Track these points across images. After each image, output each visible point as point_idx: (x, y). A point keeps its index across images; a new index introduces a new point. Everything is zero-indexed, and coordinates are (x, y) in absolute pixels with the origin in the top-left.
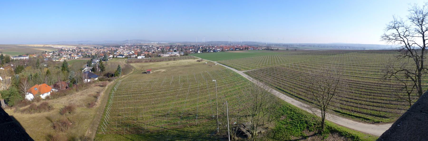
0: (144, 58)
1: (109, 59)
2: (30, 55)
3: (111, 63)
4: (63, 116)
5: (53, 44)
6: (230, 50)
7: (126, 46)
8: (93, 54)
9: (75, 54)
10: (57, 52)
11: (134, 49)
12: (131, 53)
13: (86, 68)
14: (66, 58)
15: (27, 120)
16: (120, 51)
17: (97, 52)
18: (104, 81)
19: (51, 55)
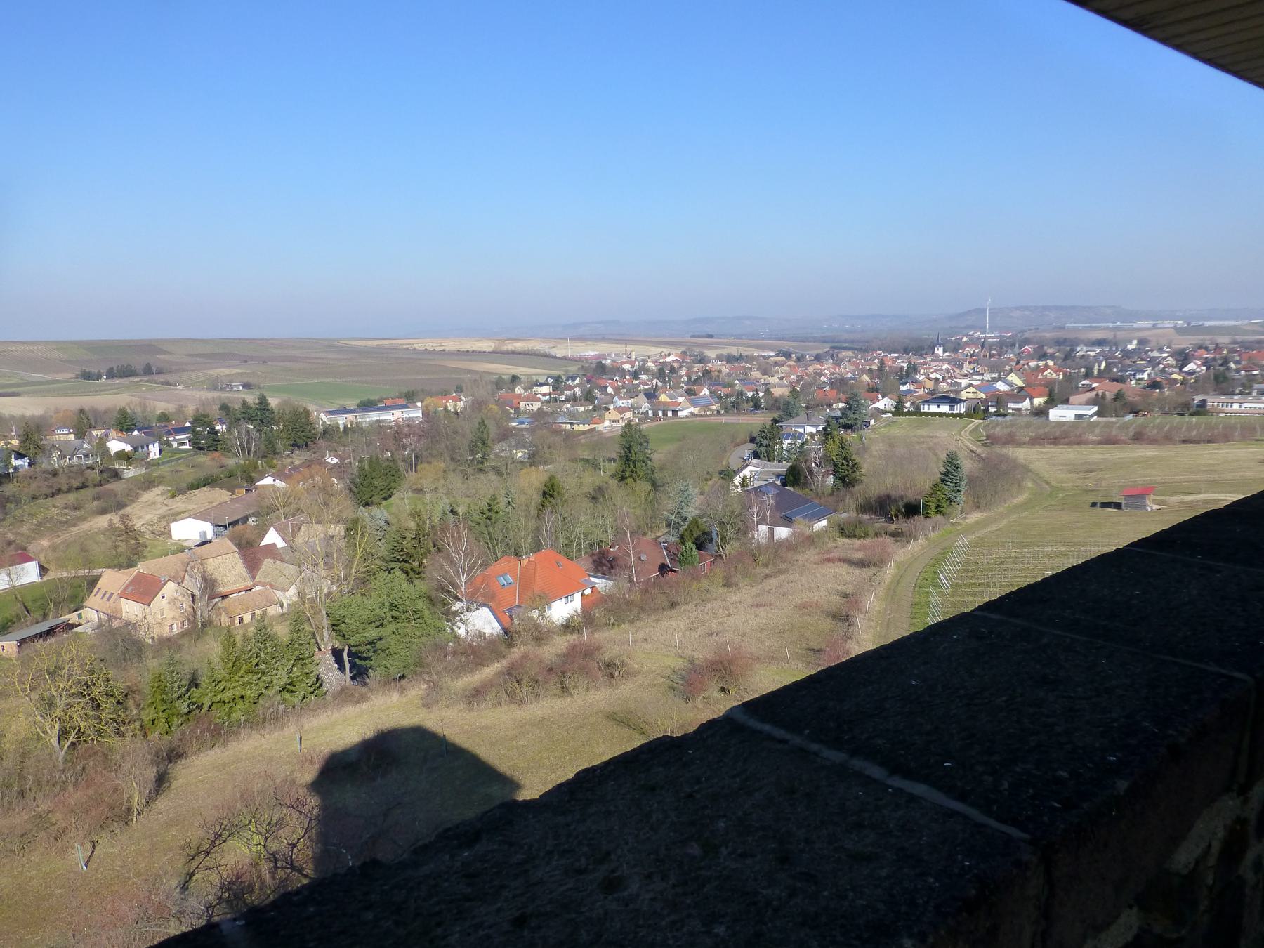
0: (1092, 416)
1: (872, 422)
2: (428, 401)
3: (891, 443)
4: (690, 705)
5: (545, 339)
7: (967, 344)
8: (777, 392)
9: (680, 391)
10: (574, 379)
11: (1018, 363)
12: (1001, 387)
13: (749, 468)
14: (629, 415)
15: (512, 738)
16: (932, 372)
17: (799, 379)
18: (866, 535)
19: (544, 395)
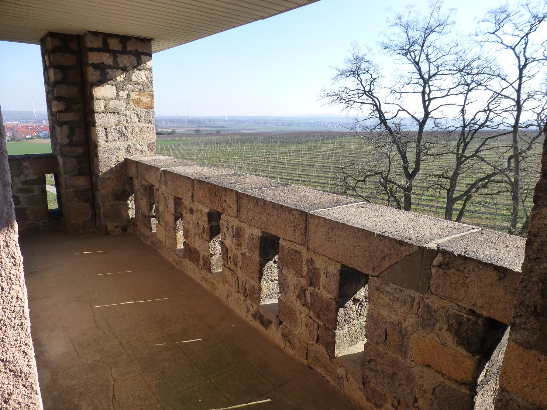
6: (40, 137)
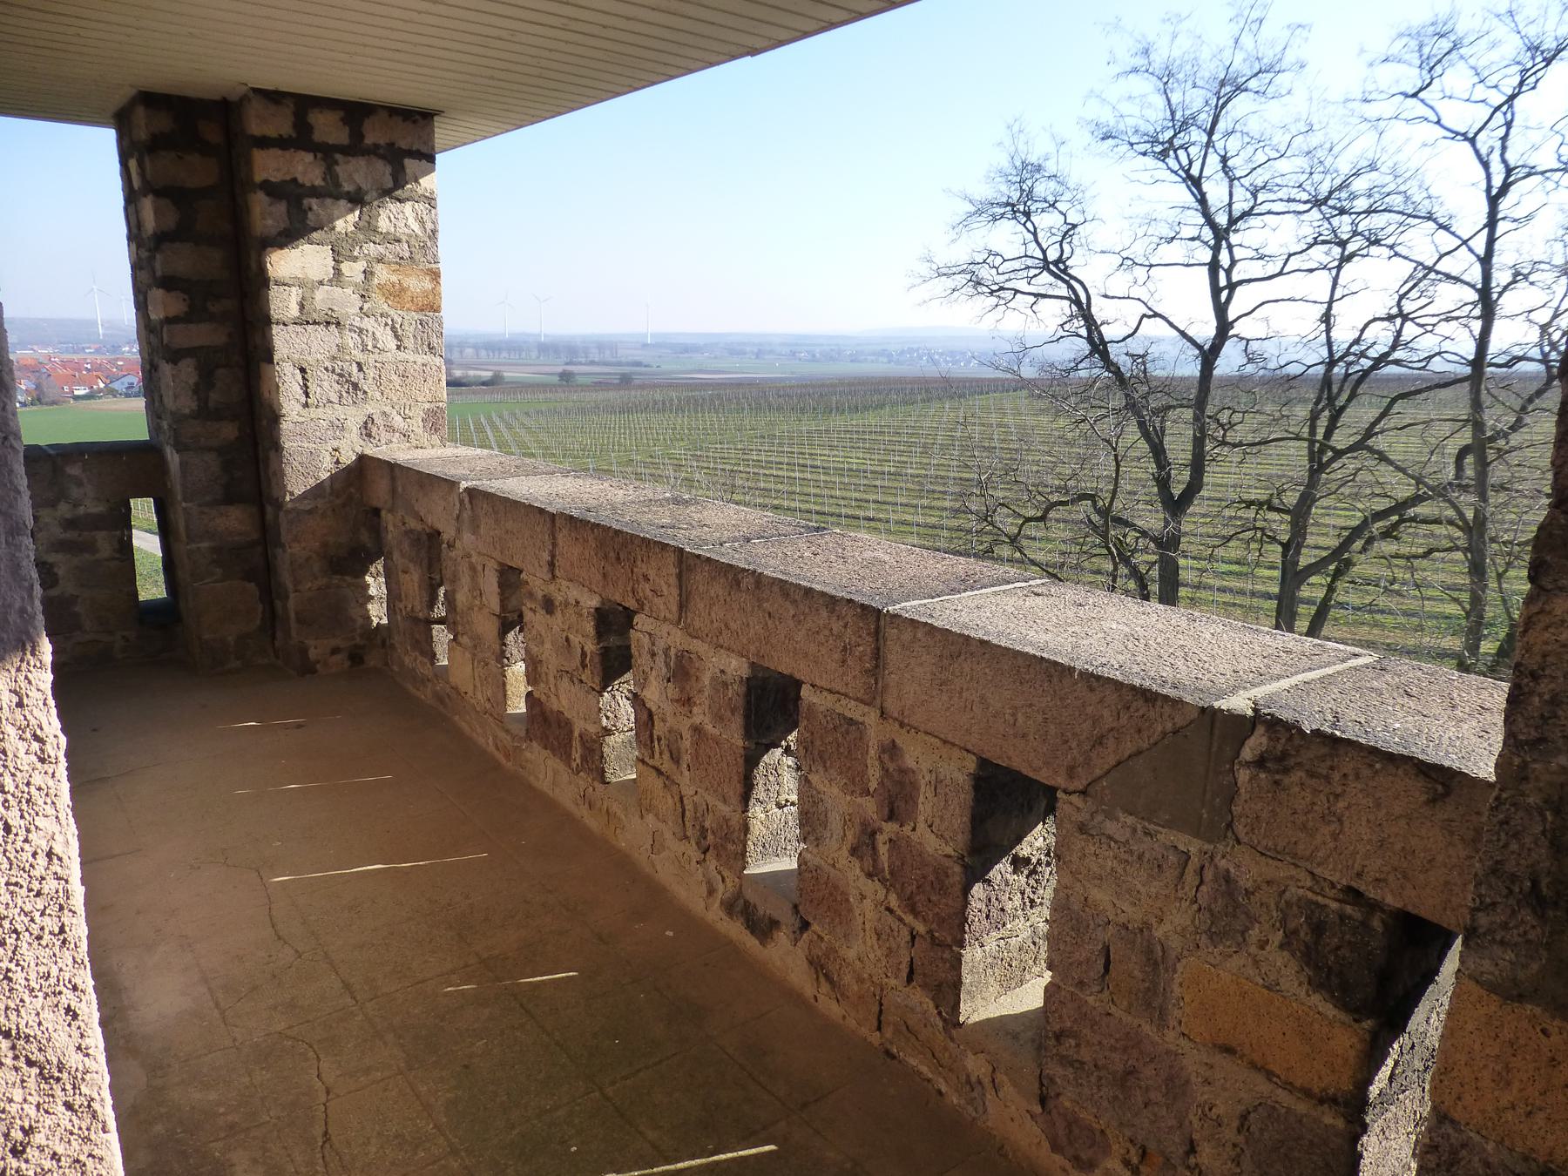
6: (114, 393)
